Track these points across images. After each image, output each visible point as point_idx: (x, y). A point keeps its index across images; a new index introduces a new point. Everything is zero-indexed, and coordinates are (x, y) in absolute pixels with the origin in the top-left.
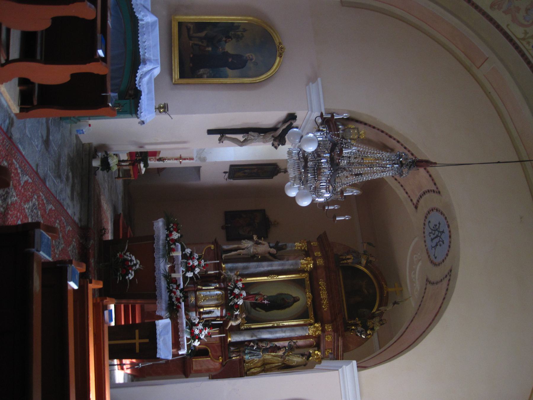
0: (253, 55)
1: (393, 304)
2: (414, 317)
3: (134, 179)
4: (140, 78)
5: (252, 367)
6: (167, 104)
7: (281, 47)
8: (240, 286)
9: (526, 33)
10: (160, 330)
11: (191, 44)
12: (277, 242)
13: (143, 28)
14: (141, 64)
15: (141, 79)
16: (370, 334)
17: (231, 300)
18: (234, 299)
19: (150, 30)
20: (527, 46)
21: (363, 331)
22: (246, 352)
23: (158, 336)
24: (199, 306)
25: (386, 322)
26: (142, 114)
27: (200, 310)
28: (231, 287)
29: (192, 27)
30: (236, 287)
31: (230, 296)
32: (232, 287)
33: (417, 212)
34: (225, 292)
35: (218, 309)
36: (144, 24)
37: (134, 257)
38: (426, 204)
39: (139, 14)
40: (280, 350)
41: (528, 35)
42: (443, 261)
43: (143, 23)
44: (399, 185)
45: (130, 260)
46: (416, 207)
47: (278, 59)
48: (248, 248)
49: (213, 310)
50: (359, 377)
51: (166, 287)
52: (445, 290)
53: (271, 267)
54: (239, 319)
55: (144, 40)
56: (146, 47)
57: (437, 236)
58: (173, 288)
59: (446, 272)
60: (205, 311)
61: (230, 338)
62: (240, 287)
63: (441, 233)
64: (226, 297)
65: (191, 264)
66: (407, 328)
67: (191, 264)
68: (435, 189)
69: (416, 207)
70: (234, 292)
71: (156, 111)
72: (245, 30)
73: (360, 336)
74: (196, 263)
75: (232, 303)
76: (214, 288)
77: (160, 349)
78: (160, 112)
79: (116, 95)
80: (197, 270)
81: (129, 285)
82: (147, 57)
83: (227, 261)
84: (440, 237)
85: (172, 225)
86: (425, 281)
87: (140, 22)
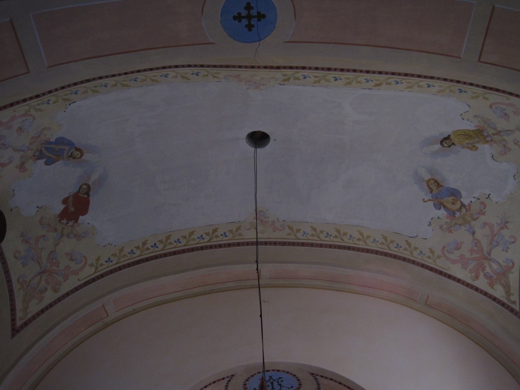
9: (91, 265)
20: (104, 267)
41: (95, 264)
42: (299, 380)
57: (272, 384)
59: (311, 378)
63: (271, 379)
84: (274, 380)
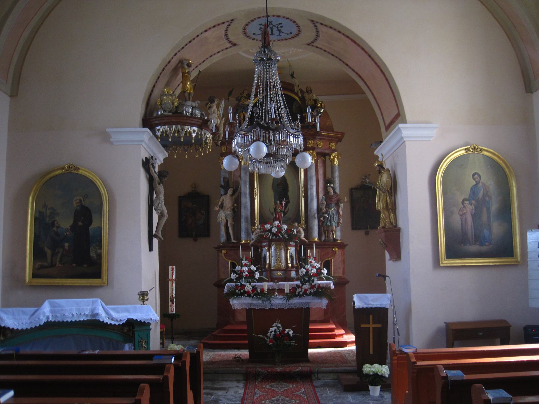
0: (75, 199)
1: (293, 78)
2: (343, 62)
3: (164, 329)
4: (112, 320)
5: (389, 220)
6: (140, 292)
7: (67, 167)
8: (269, 226)
10: (363, 304)
11: (60, 265)
12: (220, 186)
13: (56, 316)
14: (97, 319)
15: (114, 319)
16: (321, 104)
17: (283, 236)
18: (281, 233)
19: (60, 309)
21: (317, 110)
22: (329, 225)
23: (369, 306)
24: (286, 268)
25: (310, 87)
26: (152, 319)
27: (290, 267)
28: (270, 235)
29: (40, 263)
30: (270, 231)
31: (279, 236)
32: (270, 234)
33: (239, 45)
34: (273, 241)
35: (290, 249)
36: (52, 316)
37: (271, 329)
38: (236, 34)
39: (41, 320)
40: (329, 192)
42: (298, 26)
43: (51, 316)
44: (210, 59)
45: (274, 332)
46: (235, 45)
47: (80, 172)
48: (226, 216)
49: (290, 254)
50: (410, 123)
51: (299, 298)
52: (330, 30)
53: (247, 194)
54: (299, 229)
55: (71, 316)
56: (79, 314)
57: (272, 29)
58: (301, 291)
60: (291, 262)
61: (315, 239)
62: (270, 227)
64: (280, 240)
65: (247, 273)
66: (354, 70)
67: (247, 273)
68: (227, 24)
69: (235, 45)
70: (275, 232)
71: (146, 304)
72: (45, 206)
73: (321, 114)
74: (245, 269)
75: (286, 236)
76: (268, 252)
77: (380, 305)
78: (147, 300)
79: (128, 345)
80: (253, 268)
81: (296, 334)
82: (89, 313)
83: (239, 239)
84: (274, 26)
85: (237, 291)
86: (309, 47)
87: (50, 319)
